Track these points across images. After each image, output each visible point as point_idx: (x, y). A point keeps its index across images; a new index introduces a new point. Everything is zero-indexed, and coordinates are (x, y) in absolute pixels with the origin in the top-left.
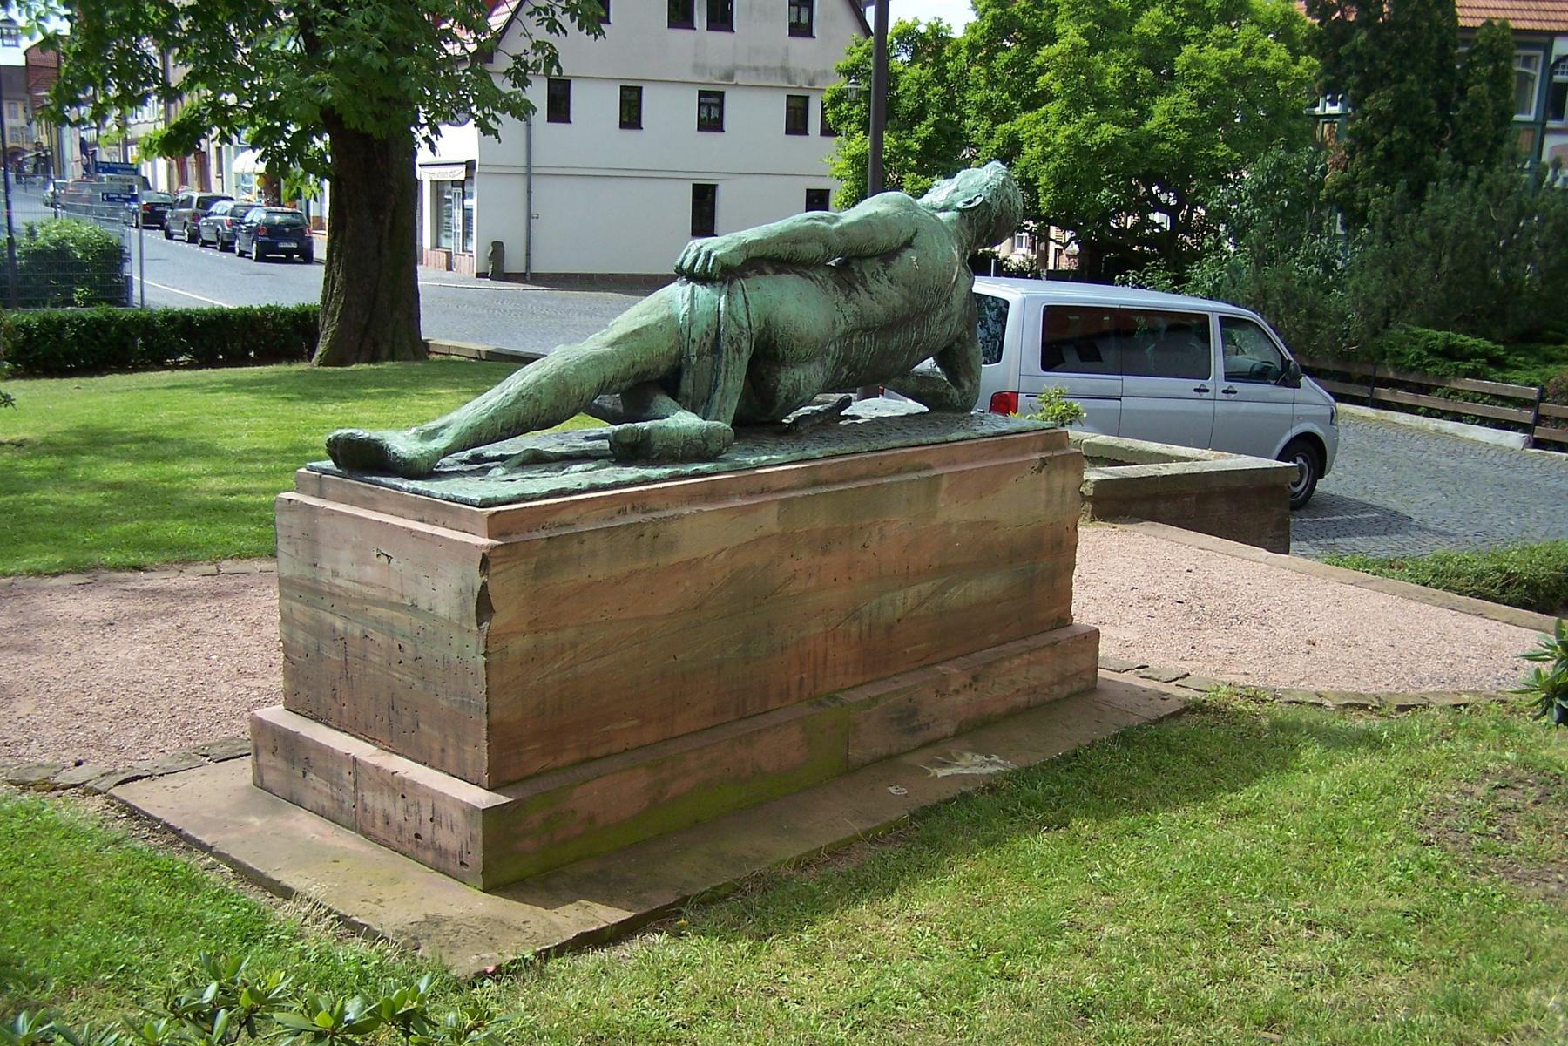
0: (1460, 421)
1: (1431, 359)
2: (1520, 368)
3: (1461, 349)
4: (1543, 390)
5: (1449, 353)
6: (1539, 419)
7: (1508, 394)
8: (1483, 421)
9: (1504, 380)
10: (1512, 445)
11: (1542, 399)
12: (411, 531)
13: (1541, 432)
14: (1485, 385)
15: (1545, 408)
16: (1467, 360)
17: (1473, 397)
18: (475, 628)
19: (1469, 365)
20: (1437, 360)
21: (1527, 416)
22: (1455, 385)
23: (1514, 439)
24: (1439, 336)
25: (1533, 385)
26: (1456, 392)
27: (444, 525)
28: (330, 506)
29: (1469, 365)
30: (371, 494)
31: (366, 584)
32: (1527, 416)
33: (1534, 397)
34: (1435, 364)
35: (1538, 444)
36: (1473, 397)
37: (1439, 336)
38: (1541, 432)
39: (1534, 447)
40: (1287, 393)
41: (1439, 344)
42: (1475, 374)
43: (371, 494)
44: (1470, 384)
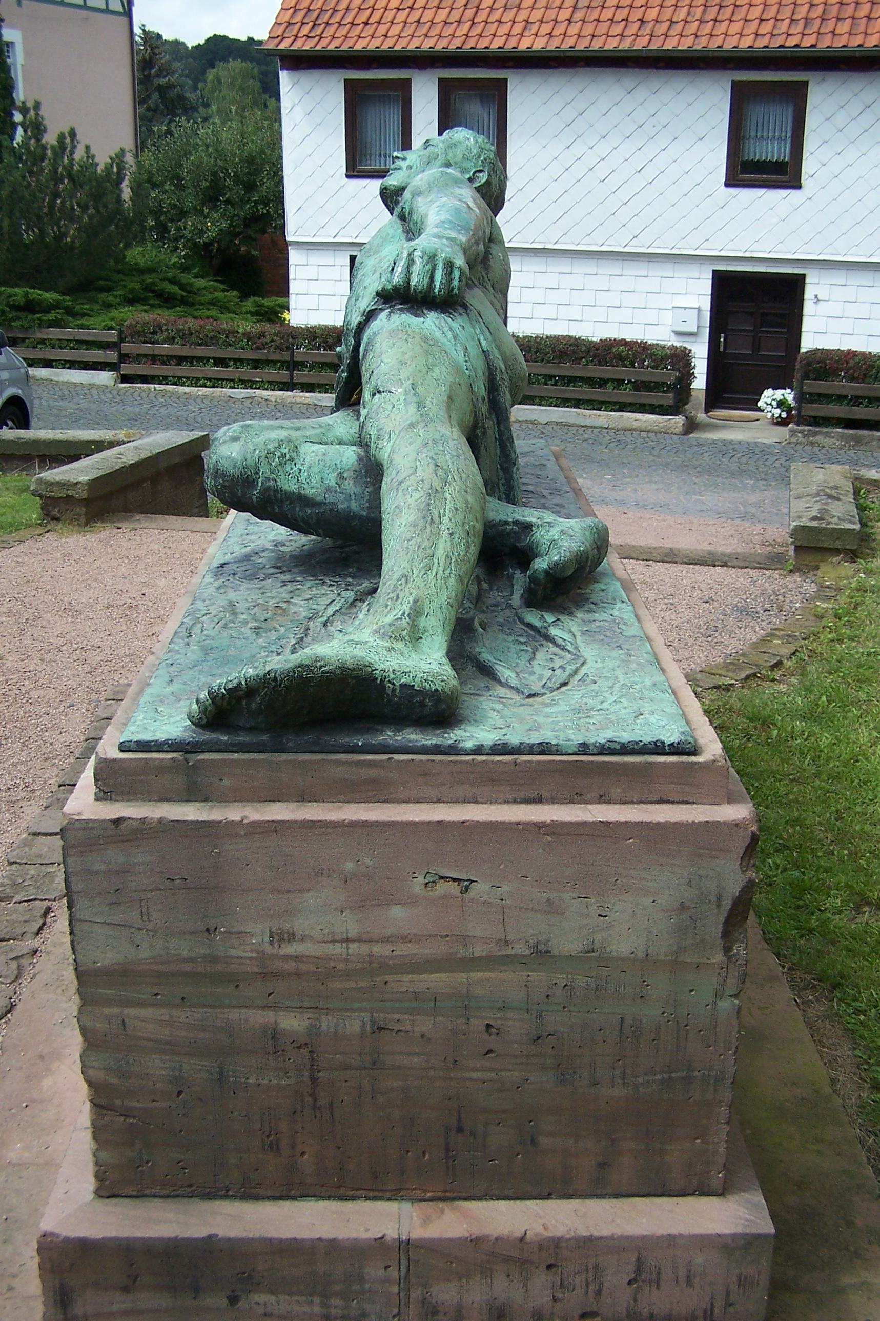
0: (52, 367)
1: (14, 314)
2: (89, 316)
3: (39, 303)
4: (121, 332)
5: (30, 307)
6: (124, 358)
7: (90, 338)
8: (72, 365)
9: (82, 327)
10: (105, 382)
11: (122, 340)
12: (539, 826)
13: (126, 369)
14: (70, 333)
15: (126, 347)
16: (48, 312)
17: (61, 344)
18: (719, 957)
19: (51, 316)
20: (19, 314)
21: (112, 356)
22: (39, 336)
23: (105, 378)
24: (19, 293)
25: (111, 328)
26: (43, 341)
27: (602, 799)
28: (233, 813)
29: (51, 316)
30: (373, 773)
31: (386, 940)
32: (112, 356)
33: (115, 339)
34: (18, 318)
35: (125, 379)
36: (61, 344)
37: (19, 293)
38: (126, 369)
39: (122, 382)
40: (314, 360)
41: (20, 299)
42: (56, 324)
43: (373, 773)
44: (54, 333)
